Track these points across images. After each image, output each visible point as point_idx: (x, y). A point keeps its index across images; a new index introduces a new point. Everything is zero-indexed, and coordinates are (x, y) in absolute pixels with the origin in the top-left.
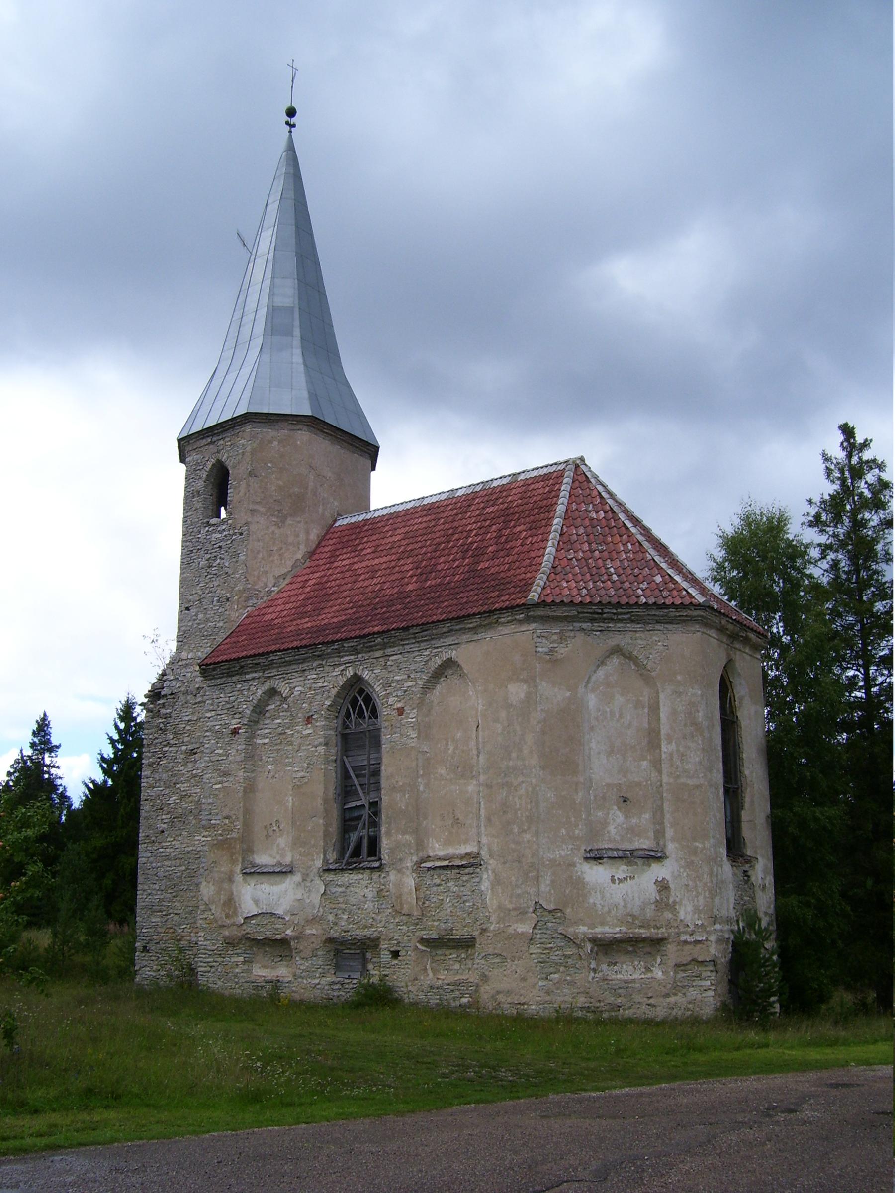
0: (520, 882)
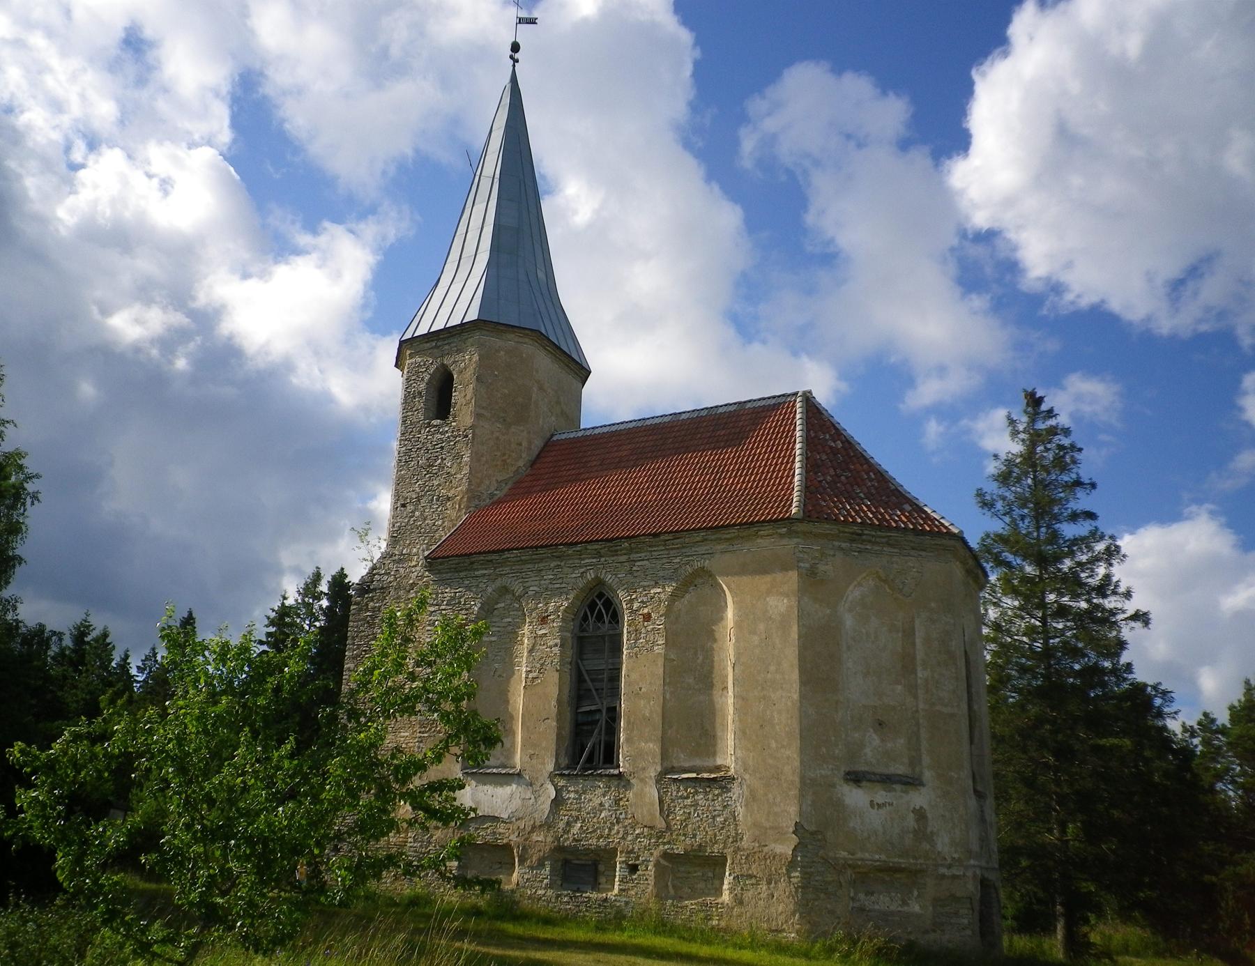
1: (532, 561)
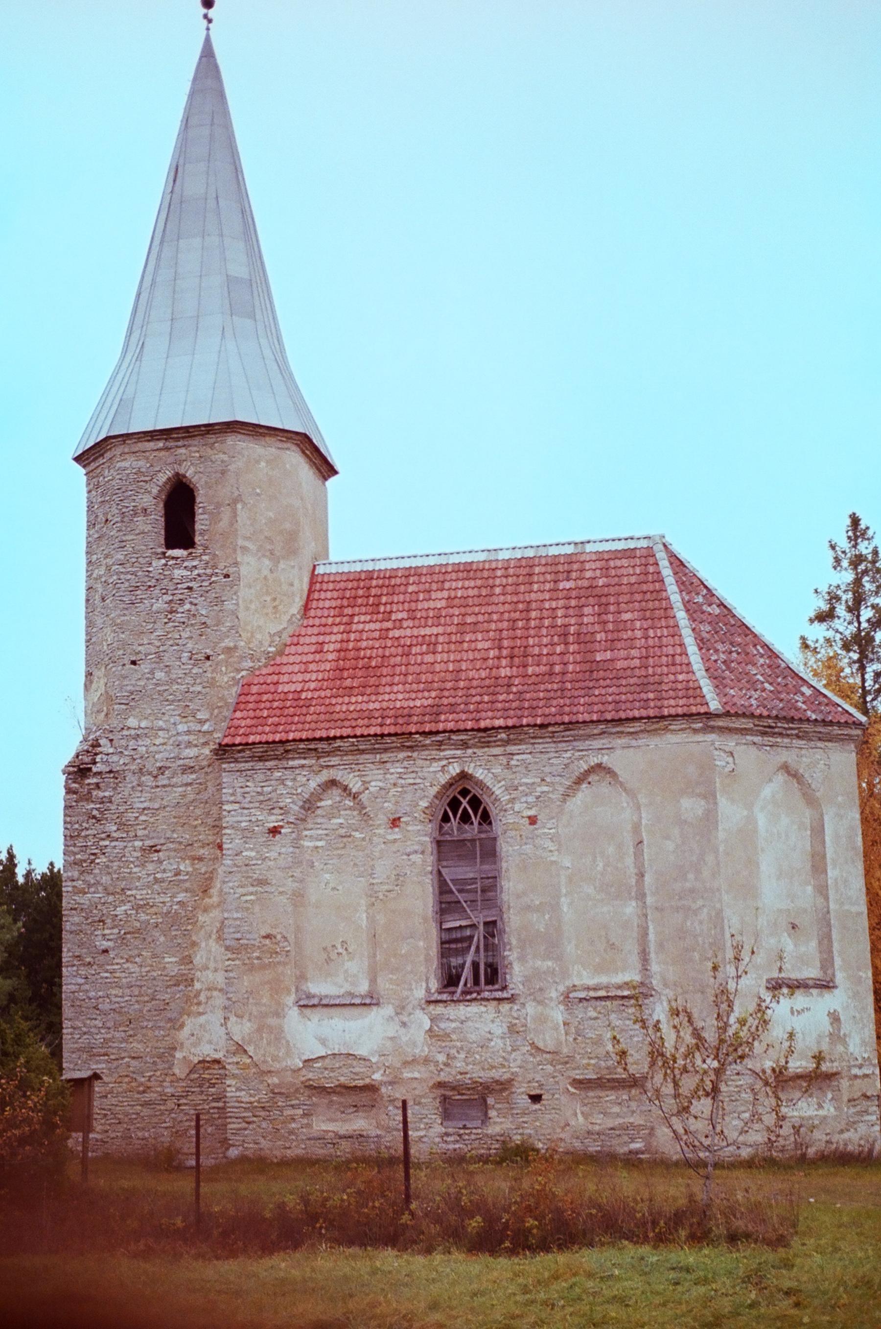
0: (705, 1014)
1: (373, 751)
